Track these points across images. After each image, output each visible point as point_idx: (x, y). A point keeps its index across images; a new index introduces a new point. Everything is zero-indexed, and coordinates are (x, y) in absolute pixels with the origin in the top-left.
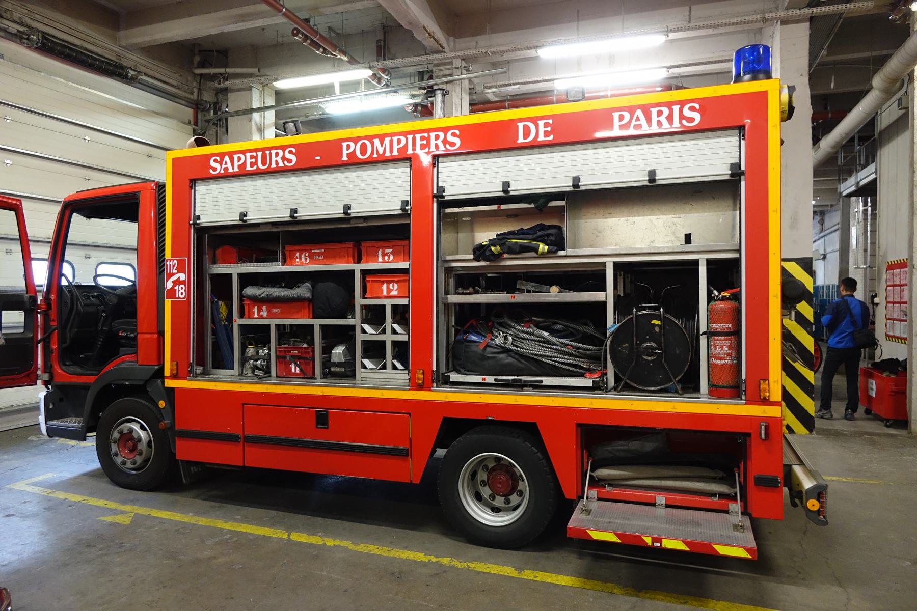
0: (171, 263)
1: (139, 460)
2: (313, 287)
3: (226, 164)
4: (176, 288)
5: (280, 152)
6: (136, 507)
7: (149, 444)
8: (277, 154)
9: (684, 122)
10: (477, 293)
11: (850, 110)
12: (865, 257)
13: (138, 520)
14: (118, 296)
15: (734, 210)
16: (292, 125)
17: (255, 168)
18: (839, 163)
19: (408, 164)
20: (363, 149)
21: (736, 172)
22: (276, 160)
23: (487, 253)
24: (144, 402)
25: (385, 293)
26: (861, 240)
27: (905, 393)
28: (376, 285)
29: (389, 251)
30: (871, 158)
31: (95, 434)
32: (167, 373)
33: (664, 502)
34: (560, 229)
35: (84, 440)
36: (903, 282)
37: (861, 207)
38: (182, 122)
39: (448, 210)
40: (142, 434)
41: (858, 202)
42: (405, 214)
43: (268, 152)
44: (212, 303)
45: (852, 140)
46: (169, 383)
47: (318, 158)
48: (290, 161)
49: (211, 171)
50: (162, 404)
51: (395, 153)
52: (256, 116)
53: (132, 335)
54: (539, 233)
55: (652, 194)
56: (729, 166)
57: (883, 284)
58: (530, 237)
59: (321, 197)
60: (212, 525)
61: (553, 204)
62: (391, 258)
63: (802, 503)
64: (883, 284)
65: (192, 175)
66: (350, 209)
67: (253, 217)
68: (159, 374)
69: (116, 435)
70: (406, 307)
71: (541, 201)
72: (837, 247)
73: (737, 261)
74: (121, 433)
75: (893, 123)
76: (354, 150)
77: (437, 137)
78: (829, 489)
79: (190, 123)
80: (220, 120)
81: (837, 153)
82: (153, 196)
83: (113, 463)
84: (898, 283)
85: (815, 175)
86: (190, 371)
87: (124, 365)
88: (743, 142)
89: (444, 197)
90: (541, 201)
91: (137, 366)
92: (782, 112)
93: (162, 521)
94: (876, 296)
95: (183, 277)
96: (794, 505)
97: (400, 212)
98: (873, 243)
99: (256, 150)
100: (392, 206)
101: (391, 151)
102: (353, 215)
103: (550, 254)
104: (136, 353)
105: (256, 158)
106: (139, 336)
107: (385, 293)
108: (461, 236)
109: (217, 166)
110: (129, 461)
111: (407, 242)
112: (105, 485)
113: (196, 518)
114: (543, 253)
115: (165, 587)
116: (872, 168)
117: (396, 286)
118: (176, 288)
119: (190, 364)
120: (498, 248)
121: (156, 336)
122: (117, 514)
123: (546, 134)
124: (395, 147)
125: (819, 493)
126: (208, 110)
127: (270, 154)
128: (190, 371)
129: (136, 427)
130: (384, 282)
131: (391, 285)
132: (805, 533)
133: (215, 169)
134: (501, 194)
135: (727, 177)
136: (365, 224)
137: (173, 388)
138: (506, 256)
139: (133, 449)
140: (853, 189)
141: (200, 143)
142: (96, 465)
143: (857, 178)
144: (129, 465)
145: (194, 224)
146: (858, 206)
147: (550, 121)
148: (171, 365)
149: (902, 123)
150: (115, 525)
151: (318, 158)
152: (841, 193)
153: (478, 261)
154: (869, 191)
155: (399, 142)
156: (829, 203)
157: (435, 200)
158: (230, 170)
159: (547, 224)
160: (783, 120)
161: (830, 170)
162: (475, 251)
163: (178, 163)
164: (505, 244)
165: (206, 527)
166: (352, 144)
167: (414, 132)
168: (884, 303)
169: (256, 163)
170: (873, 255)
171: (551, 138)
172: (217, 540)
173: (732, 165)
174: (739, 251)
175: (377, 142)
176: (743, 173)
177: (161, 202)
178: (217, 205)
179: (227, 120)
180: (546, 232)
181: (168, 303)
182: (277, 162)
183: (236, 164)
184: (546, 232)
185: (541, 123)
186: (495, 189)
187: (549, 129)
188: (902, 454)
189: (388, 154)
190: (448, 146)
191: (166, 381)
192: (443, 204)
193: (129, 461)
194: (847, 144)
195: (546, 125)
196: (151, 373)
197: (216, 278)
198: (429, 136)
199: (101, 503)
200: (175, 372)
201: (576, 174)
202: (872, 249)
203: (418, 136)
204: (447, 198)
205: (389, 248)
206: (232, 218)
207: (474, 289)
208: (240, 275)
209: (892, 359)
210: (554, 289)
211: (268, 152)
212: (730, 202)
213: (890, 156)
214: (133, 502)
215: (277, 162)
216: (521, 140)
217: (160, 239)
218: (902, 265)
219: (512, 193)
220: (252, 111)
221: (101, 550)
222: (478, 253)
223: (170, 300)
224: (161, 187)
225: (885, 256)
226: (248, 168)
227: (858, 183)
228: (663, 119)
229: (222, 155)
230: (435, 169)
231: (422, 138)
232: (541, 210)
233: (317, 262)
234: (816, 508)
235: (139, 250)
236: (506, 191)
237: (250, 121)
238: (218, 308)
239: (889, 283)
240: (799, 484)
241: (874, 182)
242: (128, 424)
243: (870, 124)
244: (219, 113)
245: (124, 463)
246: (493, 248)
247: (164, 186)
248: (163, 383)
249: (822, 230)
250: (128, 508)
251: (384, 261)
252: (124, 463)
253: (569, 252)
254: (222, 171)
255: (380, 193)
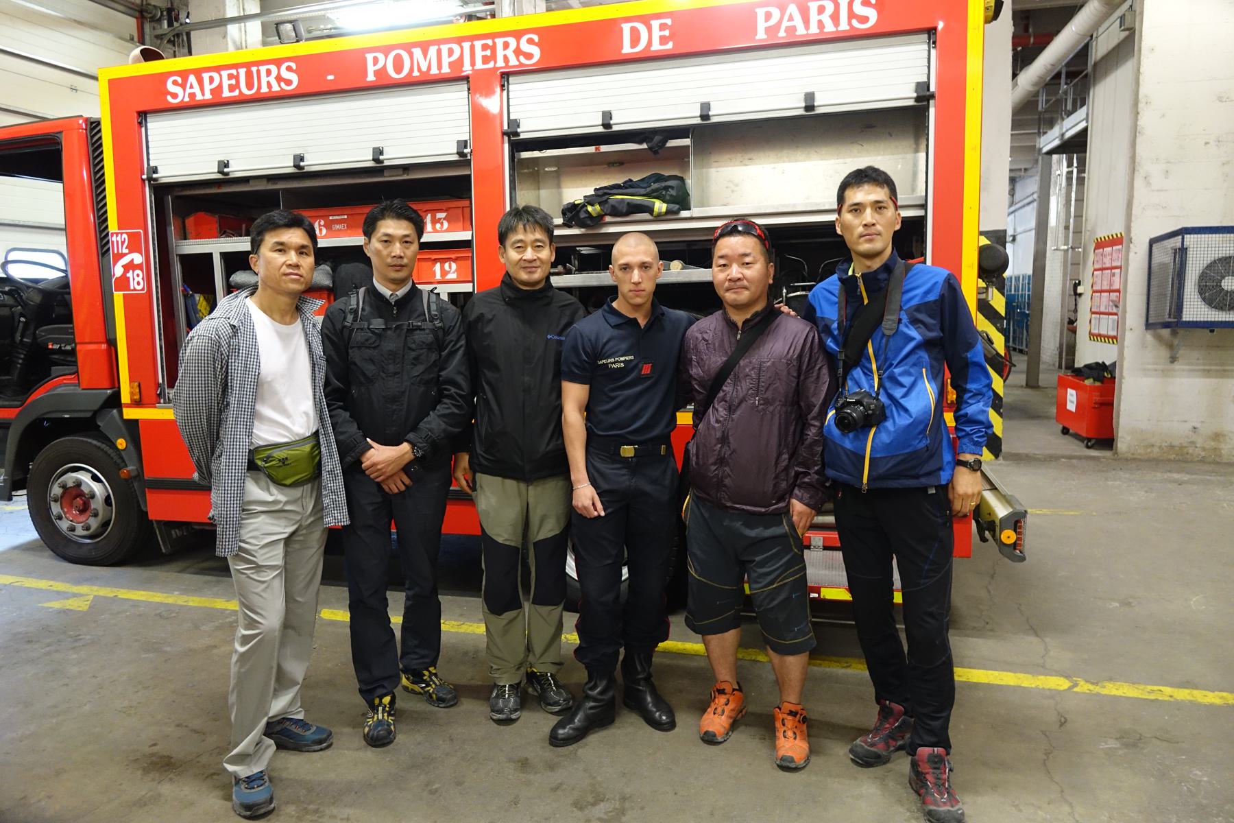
0: (118, 238)
1: (94, 523)
2: (334, 270)
3: (191, 87)
4: (130, 275)
5: (273, 68)
6: (95, 588)
7: (107, 500)
8: (269, 72)
9: (855, 23)
10: (568, 272)
11: (1058, 32)
12: (1067, 237)
13: (99, 605)
14: (40, 291)
15: (917, 151)
16: (289, 26)
17: (236, 93)
18: (1040, 108)
19: (465, 87)
20: (398, 66)
21: (924, 96)
22: (268, 82)
23: (582, 215)
24: (95, 442)
25: (438, 277)
26: (1063, 215)
27: (1112, 404)
28: (424, 264)
29: (443, 215)
30: (1081, 100)
31: (25, 492)
32: (125, 398)
33: (821, 543)
34: (682, 180)
35: (10, 499)
36: (1115, 264)
37: (1065, 170)
38: (121, 38)
39: (525, 155)
40: (96, 488)
41: (1060, 162)
42: (463, 161)
43: (254, 69)
44: (186, 296)
45: (1058, 76)
46: (130, 414)
47: (331, 77)
48: (289, 82)
49: (169, 98)
50: (121, 443)
51: (446, 69)
52: (232, 29)
53: (69, 348)
54: (655, 186)
55: (810, 127)
56: (913, 86)
57: (1090, 268)
58: (642, 191)
59: (337, 137)
60: (207, 605)
61: (673, 143)
62: (446, 225)
63: (994, 536)
64: (1090, 268)
65: (140, 106)
66: (381, 153)
67: (238, 168)
68: (114, 401)
69: (56, 490)
70: (467, 295)
71: (657, 138)
72: (1033, 224)
73: (921, 221)
74: (64, 487)
75: (1114, 49)
76: (385, 67)
77: (506, 45)
78: (1029, 519)
79: (132, 39)
80: (178, 35)
81: (1036, 94)
82: (83, 143)
83: (57, 531)
84: (1108, 265)
85: (1016, 124)
86: (159, 395)
87: (59, 391)
88: (933, 52)
89: (517, 134)
90: (657, 138)
91: (79, 390)
92: (987, 9)
93: (135, 604)
94: (1079, 284)
95: (138, 258)
96: (984, 539)
97: (456, 158)
98: (1079, 216)
99: (236, 66)
100: (446, 150)
101: (440, 67)
102: (386, 163)
103: (670, 215)
104: (77, 372)
105: (237, 77)
106: (78, 347)
107: (438, 277)
108: (544, 193)
109: (178, 90)
110: (79, 527)
111: (466, 203)
112: (48, 560)
113: (185, 598)
114: (660, 215)
115: (147, 688)
116: (1081, 113)
117: (454, 265)
118: (130, 275)
119: (158, 385)
120: (598, 207)
121: (104, 346)
122: (68, 599)
123: (663, 40)
124: (446, 61)
125: (1016, 521)
126: (160, 20)
127: (258, 71)
128: (159, 395)
129: (85, 478)
130: (436, 260)
131: (447, 266)
132: (992, 577)
133: (175, 96)
134: (601, 129)
135: (911, 103)
136: (405, 177)
137: (137, 421)
138: (608, 219)
139: (84, 509)
140: (1057, 142)
141: (148, 55)
142: (32, 534)
143: (1061, 128)
144: (80, 531)
145: (150, 179)
146: (1060, 167)
147: (669, 21)
148: (131, 387)
149: (1127, 47)
150: (66, 612)
151: (331, 77)
152: (1040, 149)
153: (570, 227)
154: (1076, 146)
155: (451, 52)
156: (1023, 167)
157: (506, 138)
158: (199, 97)
159: (666, 173)
160: (988, 21)
161: (1031, 115)
162: (564, 213)
163: (116, 86)
164: (606, 201)
165: (201, 608)
166: (381, 56)
167: (472, 38)
168: (1089, 293)
169: (237, 85)
170: (1078, 232)
171: (670, 46)
172: (216, 624)
173: (918, 84)
174: (924, 206)
175: (417, 52)
176: (932, 96)
177: (97, 147)
178: (184, 150)
179: (188, 35)
180: (664, 184)
181: (118, 297)
182: (269, 84)
183: (208, 87)
184: (664, 184)
185: (655, 24)
186: (590, 123)
187: (667, 33)
188: (1106, 479)
189: (434, 71)
190: (522, 58)
191: (125, 411)
192: (519, 145)
193: (79, 527)
194: (1052, 82)
195: (663, 27)
196: (104, 398)
197: (187, 260)
198: (494, 43)
199: (43, 584)
200: (137, 397)
201: (705, 100)
202: (1076, 224)
203: (478, 44)
204: (523, 136)
205: (441, 211)
206: (205, 169)
207: (565, 267)
208: (225, 256)
209: (1097, 364)
210: (676, 265)
211: (254, 69)
212: (908, 143)
213: (1106, 95)
214: (90, 581)
215: (269, 84)
216: (627, 49)
217: (99, 210)
218: (1115, 241)
219: (615, 128)
220: (225, 22)
221: (49, 645)
222: (569, 215)
223: (121, 293)
224: (94, 126)
225: (1093, 231)
226: (226, 93)
227: (1063, 135)
228: (826, 18)
229: (184, 74)
230: (505, 93)
231: (485, 47)
232: (656, 153)
233: (338, 234)
234: (1011, 541)
235: (68, 229)
236: (607, 125)
237: (225, 37)
238: (195, 305)
239: (1097, 266)
240: (991, 513)
241: (1084, 133)
242: (74, 475)
243: (1083, 53)
244: (176, 24)
245: (73, 529)
246: (590, 208)
247: (98, 123)
248: (121, 414)
249: (1012, 204)
250: (83, 589)
251: (435, 231)
252: (73, 529)
253: (695, 211)
254: (187, 99)
255: (424, 130)
